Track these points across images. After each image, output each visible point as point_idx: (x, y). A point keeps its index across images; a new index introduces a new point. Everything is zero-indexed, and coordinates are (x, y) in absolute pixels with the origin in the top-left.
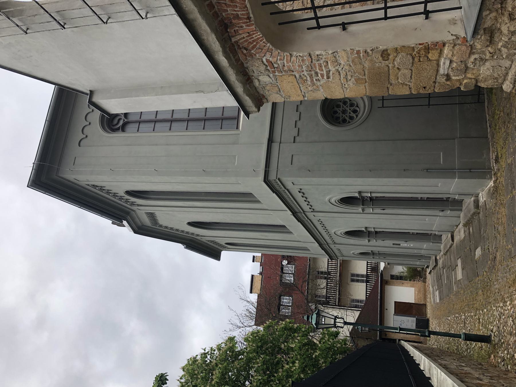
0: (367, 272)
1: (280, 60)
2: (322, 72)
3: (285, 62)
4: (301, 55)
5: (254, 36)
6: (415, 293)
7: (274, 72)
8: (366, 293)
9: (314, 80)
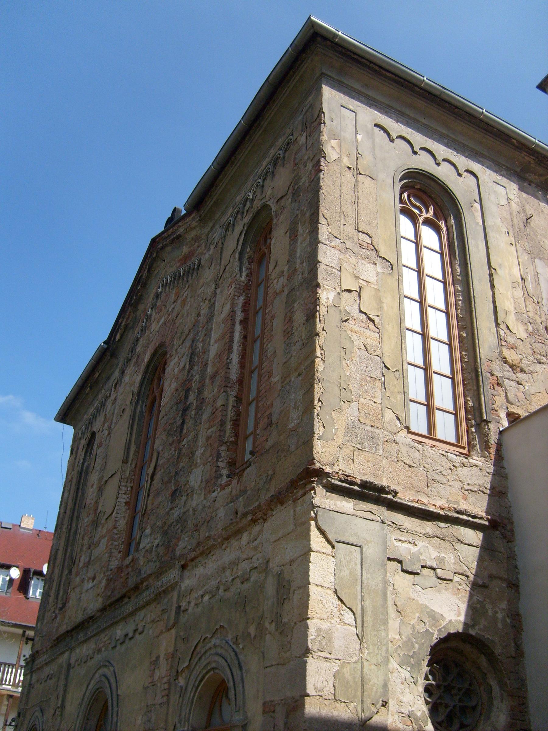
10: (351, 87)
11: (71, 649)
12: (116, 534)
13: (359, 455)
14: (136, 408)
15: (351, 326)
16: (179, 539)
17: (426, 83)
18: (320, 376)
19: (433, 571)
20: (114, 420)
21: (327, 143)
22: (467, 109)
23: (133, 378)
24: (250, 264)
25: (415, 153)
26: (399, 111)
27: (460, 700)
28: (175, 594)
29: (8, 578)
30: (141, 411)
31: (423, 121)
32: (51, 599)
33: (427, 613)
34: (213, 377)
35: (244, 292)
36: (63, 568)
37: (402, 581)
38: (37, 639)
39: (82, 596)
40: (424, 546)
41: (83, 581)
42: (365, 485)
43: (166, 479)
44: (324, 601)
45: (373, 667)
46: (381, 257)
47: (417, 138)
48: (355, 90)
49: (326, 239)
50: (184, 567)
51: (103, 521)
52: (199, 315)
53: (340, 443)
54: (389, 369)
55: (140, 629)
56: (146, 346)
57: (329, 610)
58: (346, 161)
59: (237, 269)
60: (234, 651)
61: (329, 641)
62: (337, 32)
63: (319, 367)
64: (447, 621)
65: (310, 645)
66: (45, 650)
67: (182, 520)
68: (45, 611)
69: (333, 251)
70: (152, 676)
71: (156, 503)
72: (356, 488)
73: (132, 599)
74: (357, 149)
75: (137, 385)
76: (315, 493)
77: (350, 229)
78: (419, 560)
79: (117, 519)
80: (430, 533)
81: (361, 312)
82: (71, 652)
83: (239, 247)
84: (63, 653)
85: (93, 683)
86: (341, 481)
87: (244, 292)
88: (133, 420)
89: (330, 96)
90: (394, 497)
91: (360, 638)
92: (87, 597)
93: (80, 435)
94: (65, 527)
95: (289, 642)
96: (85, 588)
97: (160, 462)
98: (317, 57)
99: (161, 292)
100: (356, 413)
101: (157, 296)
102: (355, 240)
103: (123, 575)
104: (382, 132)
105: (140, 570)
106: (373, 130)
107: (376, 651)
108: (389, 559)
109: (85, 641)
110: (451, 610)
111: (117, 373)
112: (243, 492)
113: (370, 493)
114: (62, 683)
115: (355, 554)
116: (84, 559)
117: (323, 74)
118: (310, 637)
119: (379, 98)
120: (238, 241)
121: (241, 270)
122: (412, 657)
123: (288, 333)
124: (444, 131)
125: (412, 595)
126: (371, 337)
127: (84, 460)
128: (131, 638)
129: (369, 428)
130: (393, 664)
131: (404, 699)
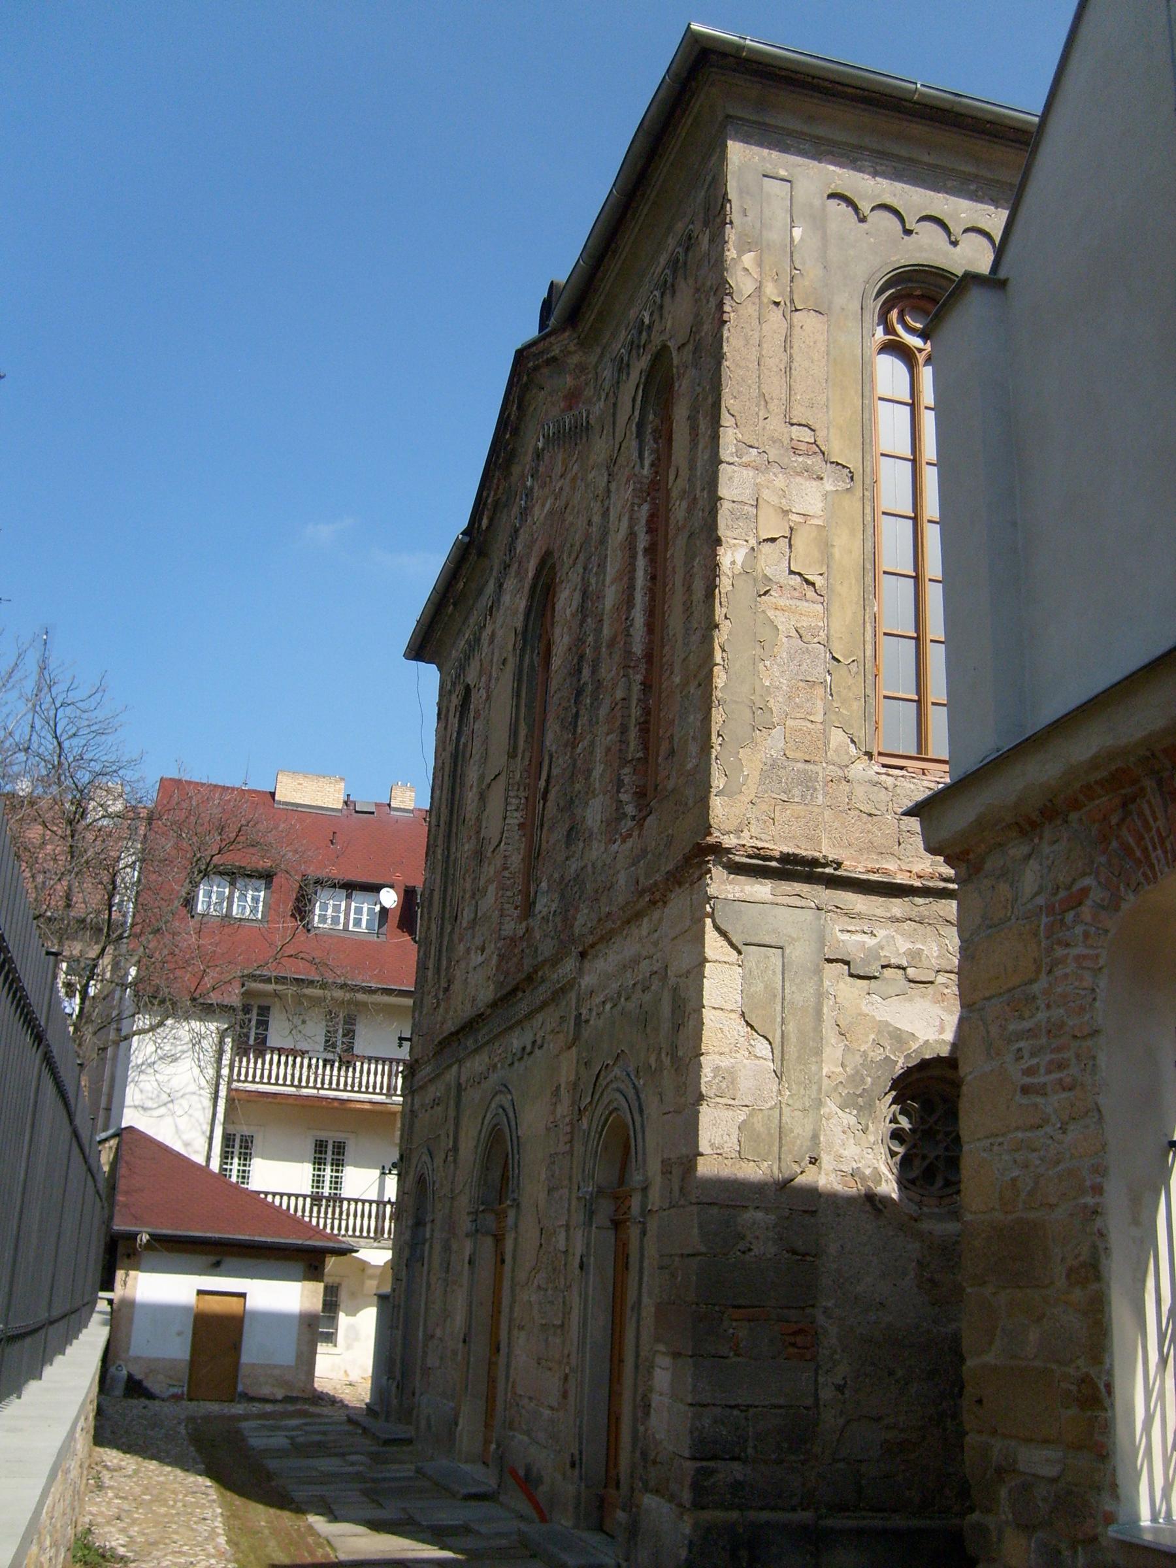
0: (349, 1200)
1: (1086, 935)
2: (1042, 1070)
3: (1075, 951)
4: (1097, 1004)
5: (1159, 852)
6: (275, 1367)
7: (1050, 909)
8: (274, 1194)
9: (1022, 1044)
10: (783, 128)
11: (460, 1062)
12: (509, 879)
13: (783, 810)
14: (521, 661)
15: (774, 600)
16: (577, 909)
17: (922, 94)
18: (720, 695)
19: (901, 971)
20: (494, 675)
21: (735, 264)
22: (1007, 122)
23: (515, 601)
24: (656, 442)
25: (908, 232)
26: (878, 152)
27: (947, 1149)
28: (573, 995)
29: (378, 908)
30: (532, 666)
31: (926, 158)
32: (430, 973)
33: (889, 1033)
34: (612, 643)
35: (649, 495)
36: (443, 923)
37: (847, 991)
38: (415, 1039)
39: (470, 975)
40: (887, 936)
41: (468, 950)
42: (785, 858)
43: (562, 804)
44: (726, 1029)
45: (797, 1113)
46: (832, 463)
47: (914, 198)
48: (790, 133)
49: (732, 454)
50: (583, 955)
51: (489, 854)
52: (590, 523)
53: (752, 796)
54: (839, 661)
55: (539, 1042)
56: (530, 546)
57: (733, 1041)
58: (771, 291)
59: (635, 454)
60: (635, 1087)
61: (732, 1083)
62: (742, 41)
63: (719, 681)
64: (921, 1042)
65: (703, 1089)
66: (426, 1058)
67: (578, 878)
68: (423, 993)
69: (745, 472)
70: (553, 1112)
71: (552, 841)
72: (774, 864)
73: (527, 993)
74: (792, 261)
75: (521, 617)
76: (711, 878)
77: (776, 425)
78: (878, 958)
79: (507, 854)
80: (899, 915)
81: (791, 572)
82: (460, 1067)
83: (637, 413)
84: (450, 1066)
85: (489, 1116)
86: (749, 856)
87: (649, 495)
88: (520, 681)
89: (742, 158)
90: (835, 869)
91: (779, 1075)
92: (476, 983)
93: (449, 687)
94: (439, 851)
95: (684, 1083)
96: (472, 964)
97: (555, 772)
98: (716, 93)
99: (543, 450)
100: (781, 745)
101: (538, 455)
102: (785, 443)
103: (516, 951)
104: (844, 205)
105: (536, 949)
106: (824, 206)
107: (802, 1091)
108: (829, 961)
109: (477, 1050)
110: (929, 1023)
111: (491, 587)
112: (644, 852)
113: (796, 869)
114: (452, 1113)
115: (773, 959)
116: (467, 916)
117: (728, 116)
118: (703, 1080)
119: (840, 136)
120: (634, 400)
121: (641, 456)
122: (860, 1096)
123: (688, 608)
124: (969, 169)
125: (865, 1009)
126: (810, 612)
127: (459, 733)
128: (530, 1053)
129: (800, 766)
130: (830, 1106)
131: (845, 1153)
